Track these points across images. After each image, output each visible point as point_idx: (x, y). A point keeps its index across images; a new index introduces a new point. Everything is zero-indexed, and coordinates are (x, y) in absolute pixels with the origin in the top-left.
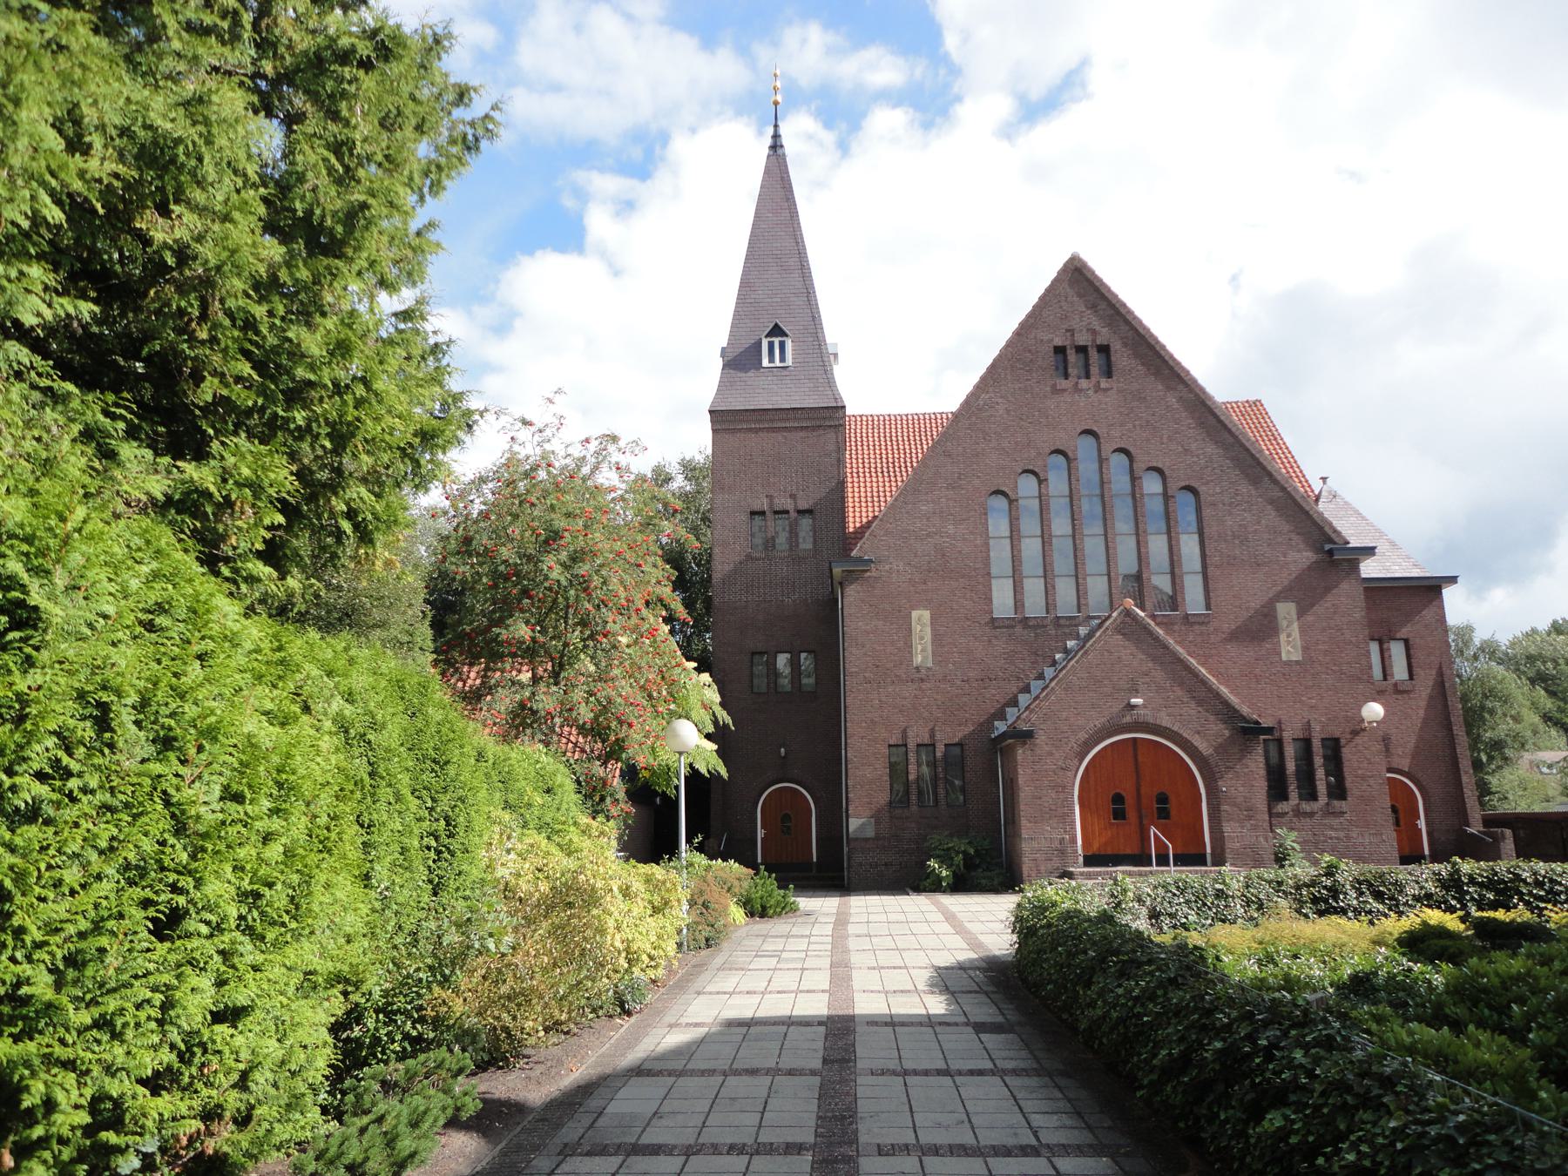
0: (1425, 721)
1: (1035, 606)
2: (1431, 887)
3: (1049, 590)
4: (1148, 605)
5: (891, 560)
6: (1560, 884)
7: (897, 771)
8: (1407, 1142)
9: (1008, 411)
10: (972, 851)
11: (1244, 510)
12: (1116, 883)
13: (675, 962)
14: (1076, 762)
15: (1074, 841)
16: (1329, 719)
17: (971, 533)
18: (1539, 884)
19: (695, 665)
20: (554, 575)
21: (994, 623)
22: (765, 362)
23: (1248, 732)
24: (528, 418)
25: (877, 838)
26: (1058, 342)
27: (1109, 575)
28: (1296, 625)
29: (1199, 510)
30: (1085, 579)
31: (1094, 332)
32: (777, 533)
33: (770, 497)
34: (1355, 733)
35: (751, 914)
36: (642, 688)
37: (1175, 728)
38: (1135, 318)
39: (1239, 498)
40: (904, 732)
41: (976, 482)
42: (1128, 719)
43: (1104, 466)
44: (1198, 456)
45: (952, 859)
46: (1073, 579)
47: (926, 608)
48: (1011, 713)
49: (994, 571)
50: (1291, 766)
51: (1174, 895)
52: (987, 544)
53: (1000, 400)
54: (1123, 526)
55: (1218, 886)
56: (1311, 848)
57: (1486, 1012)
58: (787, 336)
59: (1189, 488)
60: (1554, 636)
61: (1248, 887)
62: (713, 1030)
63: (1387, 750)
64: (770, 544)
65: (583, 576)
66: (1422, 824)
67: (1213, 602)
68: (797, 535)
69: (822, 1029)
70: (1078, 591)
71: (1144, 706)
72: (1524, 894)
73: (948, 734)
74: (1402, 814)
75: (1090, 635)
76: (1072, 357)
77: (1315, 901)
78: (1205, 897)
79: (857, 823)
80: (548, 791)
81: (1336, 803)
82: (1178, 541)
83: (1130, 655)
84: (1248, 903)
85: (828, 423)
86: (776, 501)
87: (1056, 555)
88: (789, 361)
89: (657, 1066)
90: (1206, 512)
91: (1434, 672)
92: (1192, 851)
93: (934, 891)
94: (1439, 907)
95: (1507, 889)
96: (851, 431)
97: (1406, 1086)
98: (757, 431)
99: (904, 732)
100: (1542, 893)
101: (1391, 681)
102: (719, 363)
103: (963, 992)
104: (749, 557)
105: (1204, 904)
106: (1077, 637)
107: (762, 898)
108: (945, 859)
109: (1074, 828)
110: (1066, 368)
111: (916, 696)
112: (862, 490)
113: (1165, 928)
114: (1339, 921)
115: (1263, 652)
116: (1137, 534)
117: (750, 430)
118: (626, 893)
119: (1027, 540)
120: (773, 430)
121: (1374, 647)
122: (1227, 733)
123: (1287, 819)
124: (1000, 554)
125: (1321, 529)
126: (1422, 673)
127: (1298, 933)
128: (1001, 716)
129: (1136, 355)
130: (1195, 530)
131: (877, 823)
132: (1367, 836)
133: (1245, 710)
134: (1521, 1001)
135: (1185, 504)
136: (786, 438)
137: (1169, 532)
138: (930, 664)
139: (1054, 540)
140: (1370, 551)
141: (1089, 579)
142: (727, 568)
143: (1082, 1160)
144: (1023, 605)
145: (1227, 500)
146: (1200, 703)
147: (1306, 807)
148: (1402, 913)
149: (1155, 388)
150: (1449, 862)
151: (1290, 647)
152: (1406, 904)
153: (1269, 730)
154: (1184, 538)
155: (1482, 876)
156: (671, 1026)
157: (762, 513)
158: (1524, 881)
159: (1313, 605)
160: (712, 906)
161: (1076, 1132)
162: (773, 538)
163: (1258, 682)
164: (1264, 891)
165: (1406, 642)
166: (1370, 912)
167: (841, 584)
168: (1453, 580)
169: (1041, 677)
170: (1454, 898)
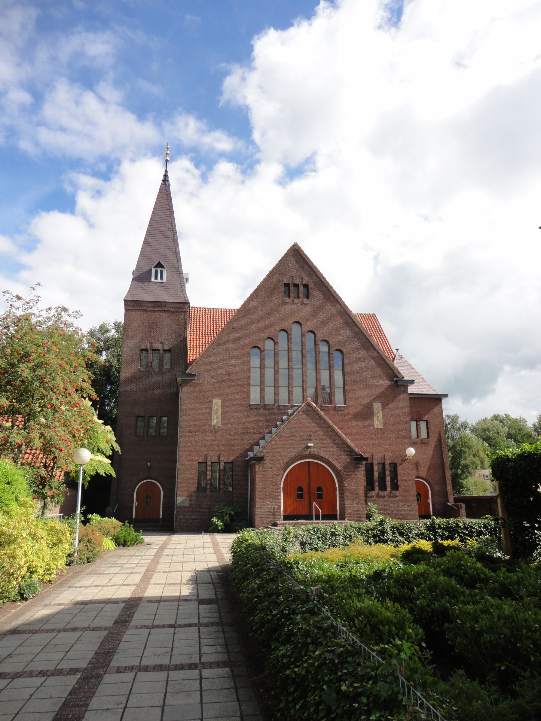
0: (433, 456)
1: (269, 400)
2: (423, 530)
3: (276, 392)
4: (319, 401)
5: (205, 375)
6: (474, 528)
7: (201, 474)
8: (319, 662)
9: (262, 311)
10: (233, 513)
11: (362, 361)
12: (285, 529)
13: (65, 571)
14: (282, 472)
15: (279, 508)
16: (393, 455)
17: (243, 365)
18: (466, 528)
19: (103, 422)
20: (25, 374)
21: (250, 406)
22: (153, 279)
23: (358, 459)
24: (20, 295)
25: (190, 507)
26: (286, 281)
27: (303, 387)
28: (381, 413)
29: (343, 360)
30: (292, 388)
31: (302, 278)
32: (153, 360)
33: (151, 343)
34: (403, 461)
35: (118, 544)
36: (70, 432)
37: (327, 457)
38: (320, 273)
39: (360, 356)
40: (206, 456)
41: (246, 342)
42: (306, 453)
43: (303, 338)
44: (343, 336)
45: (223, 517)
46: (288, 388)
47: (220, 399)
48: (256, 448)
49: (252, 383)
50: (376, 475)
51: (312, 534)
52: (249, 370)
53: (259, 305)
54: (310, 365)
55: (332, 530)
56: (382, 511)
57: (406, 590)
58: (164, 267)
59: (339, 350)
60: (494, 421)
61: (345, 530)
62: (67, 607)
63: (417, 469)
64: (149, 365)
65: (40, 376)
66: (430, 501)
67: (347, 402)
68: (163, 361)
69: (123, 605)
70: (289, 394)
71: (314, 447)
72: (460, 533)
73: (227, 458)
74: (421, 497)
75: (293, 414)
76: (292, 288)
77: (375, 536)
78: (326, 535)
79: (179, 500)
80: (9, 483)
81: (394, 492)
82: (333, 373)
83: (308, 424)
84: (346, 537)
85: (181, 310)
86: (154, 344)
87: (280, 377)
88: (164, 280)
89: (27, 628)
90: (346, 361)
91: (437, 435)
92: (331, 513)
93: (213, 532)
94: (426, 539)
95: (453, 530)
96: (192, 313)
97: (332, 633)
98: (146, 311)
99: (206, 456)
100: (467, 532)
101: (420, 439)
102: (132, 277)
103: (203, 583)
104: (139, 371)
105: (326, 539)
106: (287, 415)
107: (124, 537)
108: (221, 518)
109: (280, 503)
110: (289, 293)
111: (212, 440)
112: (198, 342)
113: (307, 550)
114: (383, 546)
115: (367, 424)
116: (316, 370)
117: (144, 310)
118: (34, 537)
119: (268, 369)
120: (155, 311)
121: (413, 424)
122: (348, 460)
123: (373, 499)
124: (255, 375)
125: (393, 371)
126: (432, 435)
127: (361, 552)
128: (251, 449)
129: (320, 290)
130: (341, 369)
131: (191, 500)
132: (406, 506)
133: (357, 450)
134: (418, 586)
135: (337, 357)
136: (160, 315)
137: (330, 369)
138: (220, 425)
139: (280, 370)
140: (412, 382)
141: (294, 388)
142: (127, 375)
143: (216, 670)
144: (264, 399)
145: (355, 357)
146: (338, 446)
147: (382, 493)
148: (411, 541)
149: (327, 305)
150: (431, 519)
151: (378, 422)
152: (412, 537)
153: (366, 459)
154: (336, 372)
155: (443, 525)
156: (45, 606)
157: (146, 350)
158: (460, 527)
159: (388, 404)
160: (92, 541)
161: (220, 655)
162: (151, 362)
163: (364, 437)
164: (353, 532)
165: (427, 421)
166: (397, 541)
167: (181, 385)
168: (446, 396)
169: (270, 432)
170: (432, 534)
